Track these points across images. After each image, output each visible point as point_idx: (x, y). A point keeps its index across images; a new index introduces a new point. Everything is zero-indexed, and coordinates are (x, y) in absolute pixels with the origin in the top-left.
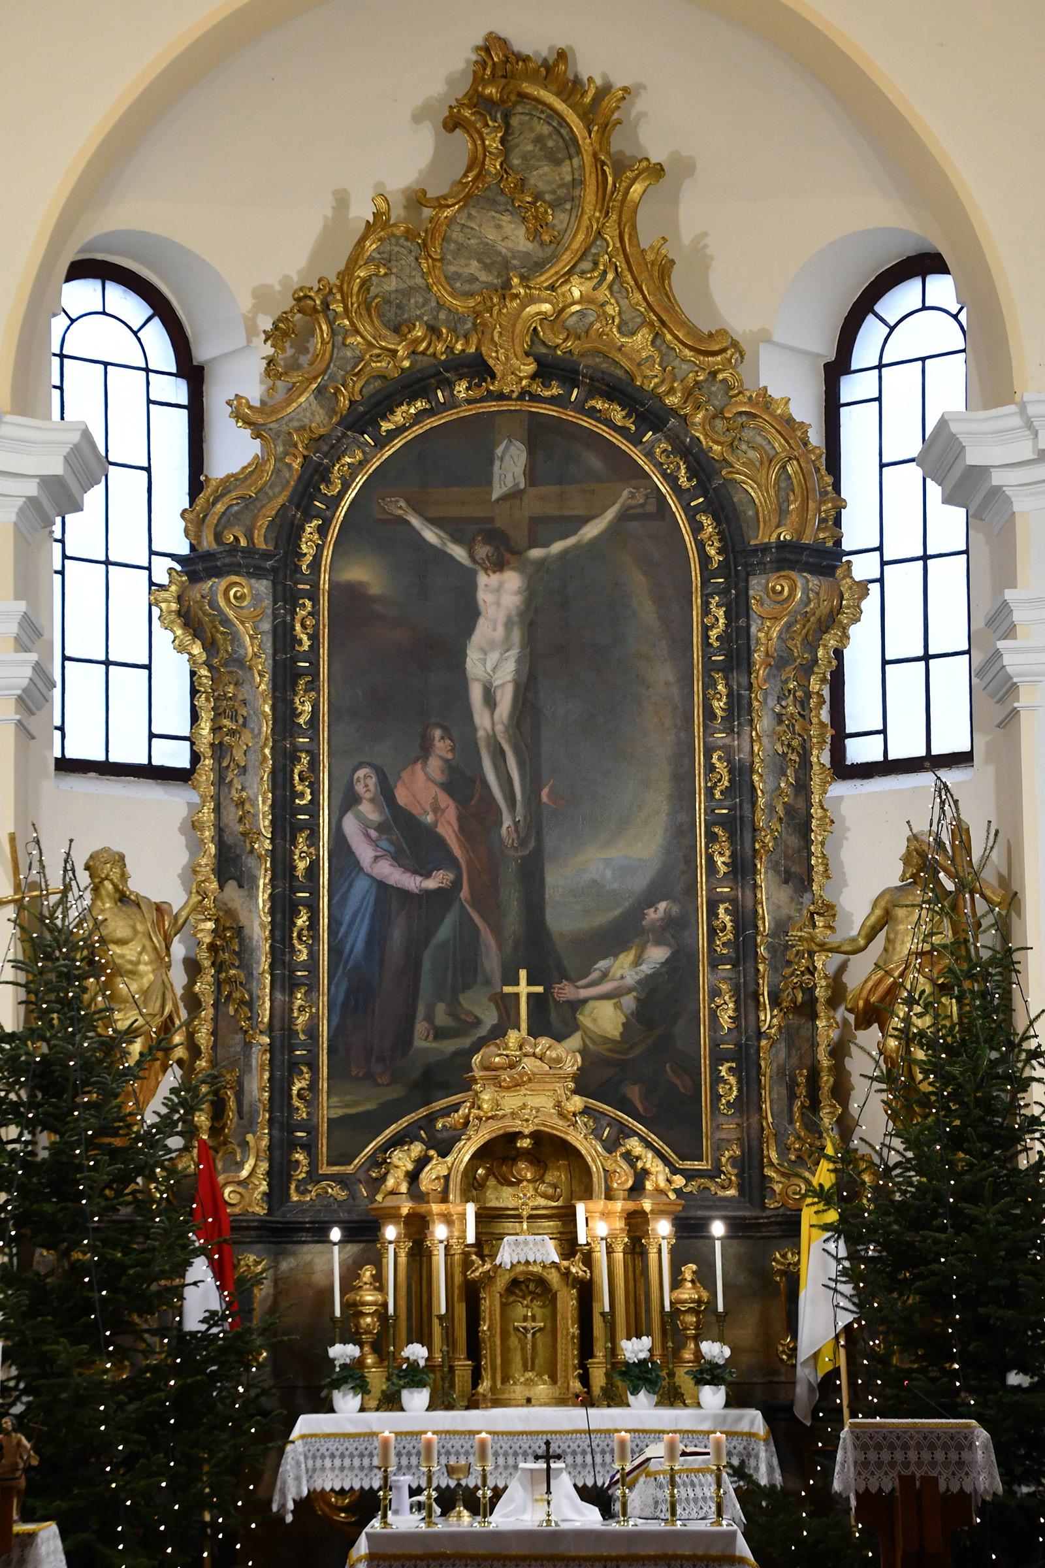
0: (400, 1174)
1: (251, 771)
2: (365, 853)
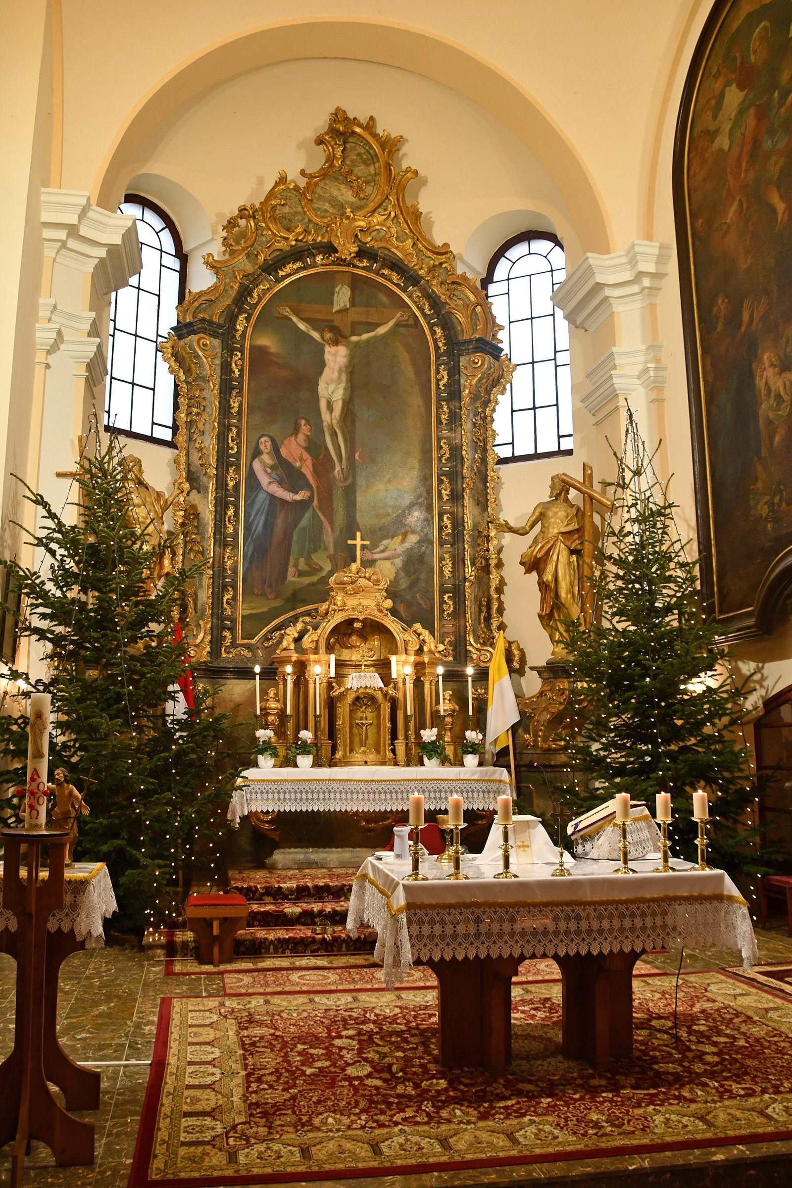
0: (290, 639)
1: (207, 433)
2: (264, 480)
